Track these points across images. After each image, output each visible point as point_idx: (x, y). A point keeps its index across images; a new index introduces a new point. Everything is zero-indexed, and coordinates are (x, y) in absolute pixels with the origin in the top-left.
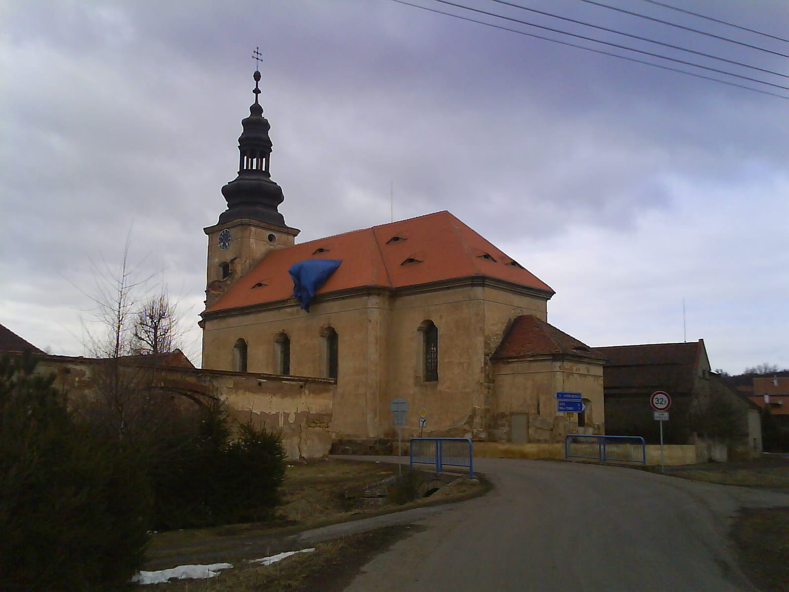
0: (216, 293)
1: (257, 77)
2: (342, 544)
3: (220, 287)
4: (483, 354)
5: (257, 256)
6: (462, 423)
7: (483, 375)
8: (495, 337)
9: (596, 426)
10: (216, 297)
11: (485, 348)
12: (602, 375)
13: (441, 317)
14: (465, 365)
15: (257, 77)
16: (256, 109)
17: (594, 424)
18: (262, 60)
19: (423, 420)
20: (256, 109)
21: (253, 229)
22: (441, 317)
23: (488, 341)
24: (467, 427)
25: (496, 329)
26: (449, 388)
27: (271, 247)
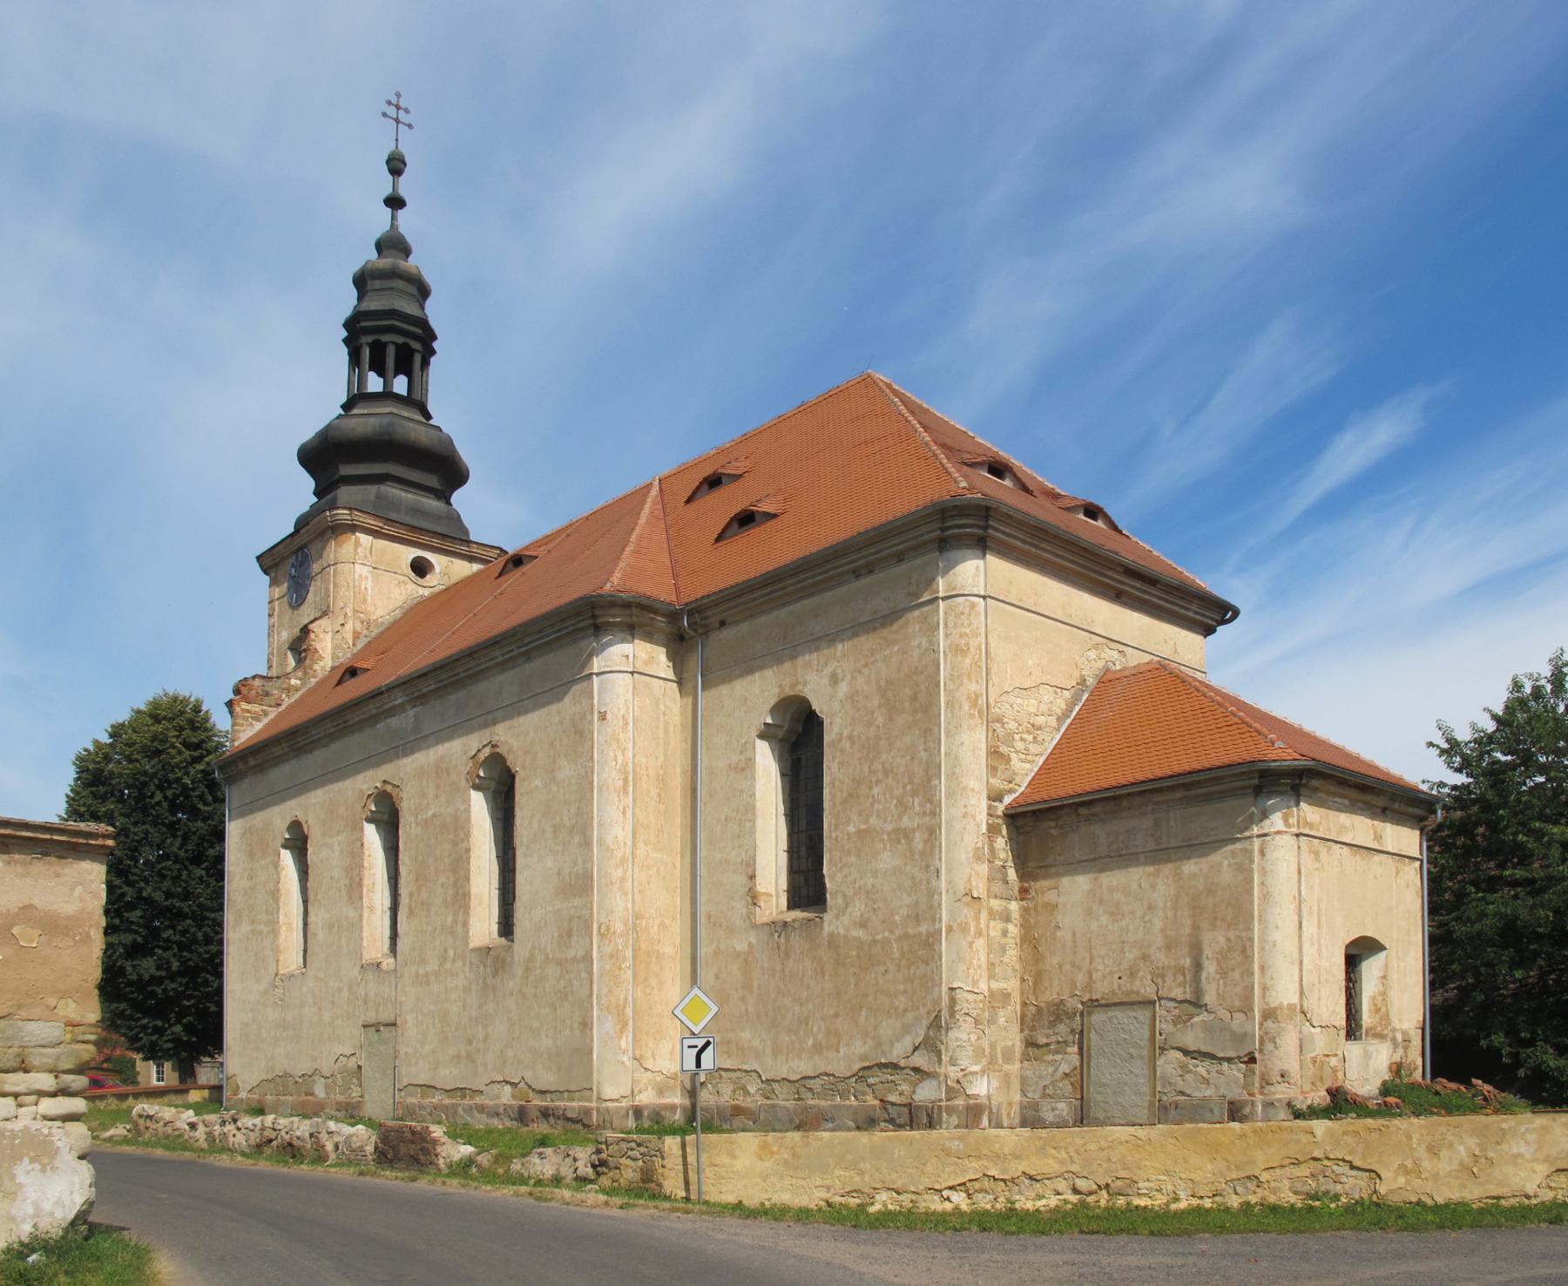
0: (256, 708)
1: (396, 166)
2: (1161, 888)
3: (267, 694)
4: (985, 795)
5: (379, 613)
6: (907, 1044)
7: (984, 868)
8: (1030, 738)
9: (1399, 1037)
10: (257, 719)
11: (993, 770)
12: (678, 1139)
13: (834, 680)
14: (918, 838)
15: (396, 166)
16: (393, 244)
17: (1394, 1030)
18: (410, 126)
19: (700, 1043)
20: (393, 244)
21: (365, 539)
22: (834, 680)
23: (1004, 749)
24: (920, 1060)
25: (1031, 704)
26: (863, 924)
27: (421, 591)
